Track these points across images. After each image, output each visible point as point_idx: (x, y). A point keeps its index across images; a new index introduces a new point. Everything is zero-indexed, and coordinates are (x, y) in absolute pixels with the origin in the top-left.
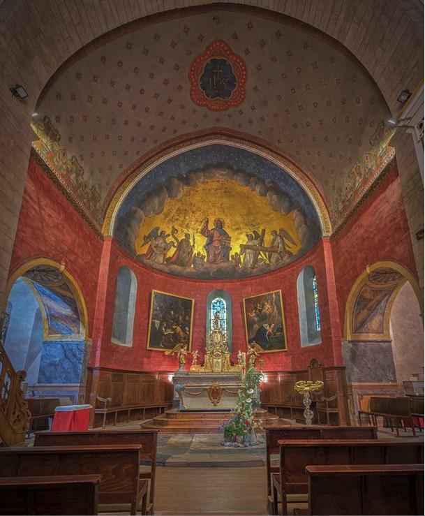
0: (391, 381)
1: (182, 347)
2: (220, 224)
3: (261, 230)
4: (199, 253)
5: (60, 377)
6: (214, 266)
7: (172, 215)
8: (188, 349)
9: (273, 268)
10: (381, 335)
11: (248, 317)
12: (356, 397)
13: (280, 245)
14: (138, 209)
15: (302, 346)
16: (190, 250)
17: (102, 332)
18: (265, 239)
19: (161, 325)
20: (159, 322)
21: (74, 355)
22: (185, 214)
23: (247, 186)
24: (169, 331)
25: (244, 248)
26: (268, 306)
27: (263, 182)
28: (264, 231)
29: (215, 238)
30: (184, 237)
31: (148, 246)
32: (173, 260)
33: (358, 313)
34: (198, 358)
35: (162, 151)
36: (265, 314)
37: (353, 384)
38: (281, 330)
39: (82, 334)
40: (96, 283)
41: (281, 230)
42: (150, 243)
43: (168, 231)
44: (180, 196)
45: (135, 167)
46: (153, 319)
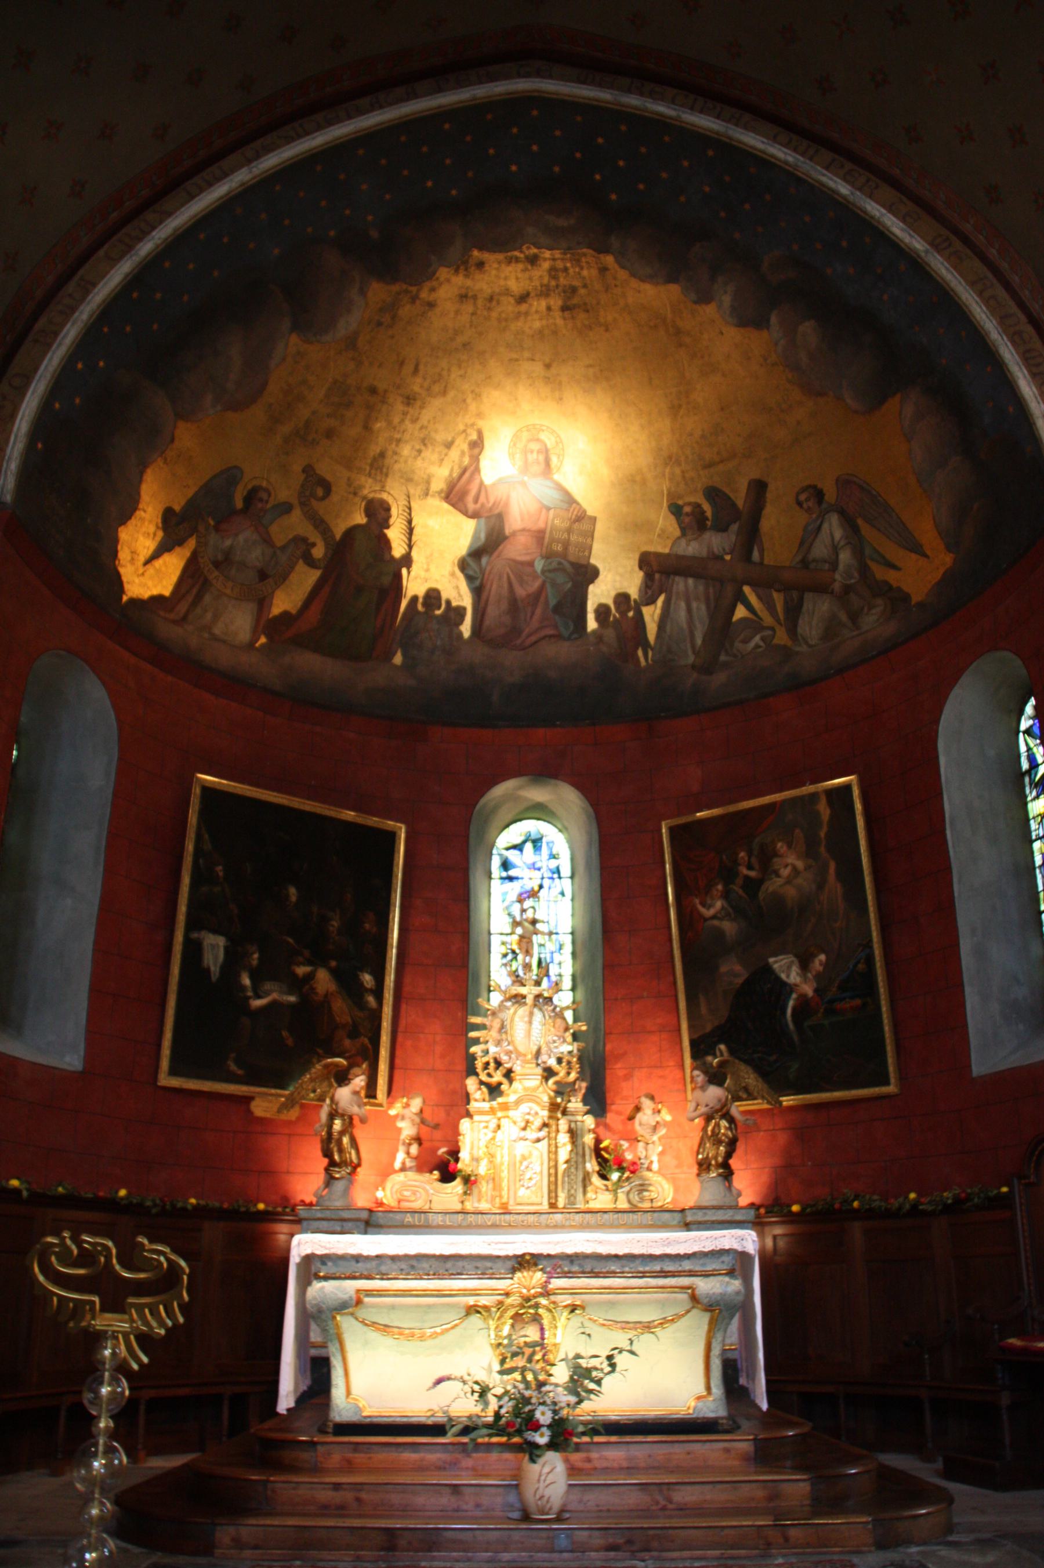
1: (343, 1078)
3: (743, 485)
4: (433, 597)
11: (688, 920)
13: (845, 557)
15: (980, 1066)
16: (386, 580)
19: (233, 960)
20: (221, 941)
23: (671, 279)
28: (759, 488)
30: (360, 519)
41: (844, 483)
44: (347, 325)
46: (192, 925)
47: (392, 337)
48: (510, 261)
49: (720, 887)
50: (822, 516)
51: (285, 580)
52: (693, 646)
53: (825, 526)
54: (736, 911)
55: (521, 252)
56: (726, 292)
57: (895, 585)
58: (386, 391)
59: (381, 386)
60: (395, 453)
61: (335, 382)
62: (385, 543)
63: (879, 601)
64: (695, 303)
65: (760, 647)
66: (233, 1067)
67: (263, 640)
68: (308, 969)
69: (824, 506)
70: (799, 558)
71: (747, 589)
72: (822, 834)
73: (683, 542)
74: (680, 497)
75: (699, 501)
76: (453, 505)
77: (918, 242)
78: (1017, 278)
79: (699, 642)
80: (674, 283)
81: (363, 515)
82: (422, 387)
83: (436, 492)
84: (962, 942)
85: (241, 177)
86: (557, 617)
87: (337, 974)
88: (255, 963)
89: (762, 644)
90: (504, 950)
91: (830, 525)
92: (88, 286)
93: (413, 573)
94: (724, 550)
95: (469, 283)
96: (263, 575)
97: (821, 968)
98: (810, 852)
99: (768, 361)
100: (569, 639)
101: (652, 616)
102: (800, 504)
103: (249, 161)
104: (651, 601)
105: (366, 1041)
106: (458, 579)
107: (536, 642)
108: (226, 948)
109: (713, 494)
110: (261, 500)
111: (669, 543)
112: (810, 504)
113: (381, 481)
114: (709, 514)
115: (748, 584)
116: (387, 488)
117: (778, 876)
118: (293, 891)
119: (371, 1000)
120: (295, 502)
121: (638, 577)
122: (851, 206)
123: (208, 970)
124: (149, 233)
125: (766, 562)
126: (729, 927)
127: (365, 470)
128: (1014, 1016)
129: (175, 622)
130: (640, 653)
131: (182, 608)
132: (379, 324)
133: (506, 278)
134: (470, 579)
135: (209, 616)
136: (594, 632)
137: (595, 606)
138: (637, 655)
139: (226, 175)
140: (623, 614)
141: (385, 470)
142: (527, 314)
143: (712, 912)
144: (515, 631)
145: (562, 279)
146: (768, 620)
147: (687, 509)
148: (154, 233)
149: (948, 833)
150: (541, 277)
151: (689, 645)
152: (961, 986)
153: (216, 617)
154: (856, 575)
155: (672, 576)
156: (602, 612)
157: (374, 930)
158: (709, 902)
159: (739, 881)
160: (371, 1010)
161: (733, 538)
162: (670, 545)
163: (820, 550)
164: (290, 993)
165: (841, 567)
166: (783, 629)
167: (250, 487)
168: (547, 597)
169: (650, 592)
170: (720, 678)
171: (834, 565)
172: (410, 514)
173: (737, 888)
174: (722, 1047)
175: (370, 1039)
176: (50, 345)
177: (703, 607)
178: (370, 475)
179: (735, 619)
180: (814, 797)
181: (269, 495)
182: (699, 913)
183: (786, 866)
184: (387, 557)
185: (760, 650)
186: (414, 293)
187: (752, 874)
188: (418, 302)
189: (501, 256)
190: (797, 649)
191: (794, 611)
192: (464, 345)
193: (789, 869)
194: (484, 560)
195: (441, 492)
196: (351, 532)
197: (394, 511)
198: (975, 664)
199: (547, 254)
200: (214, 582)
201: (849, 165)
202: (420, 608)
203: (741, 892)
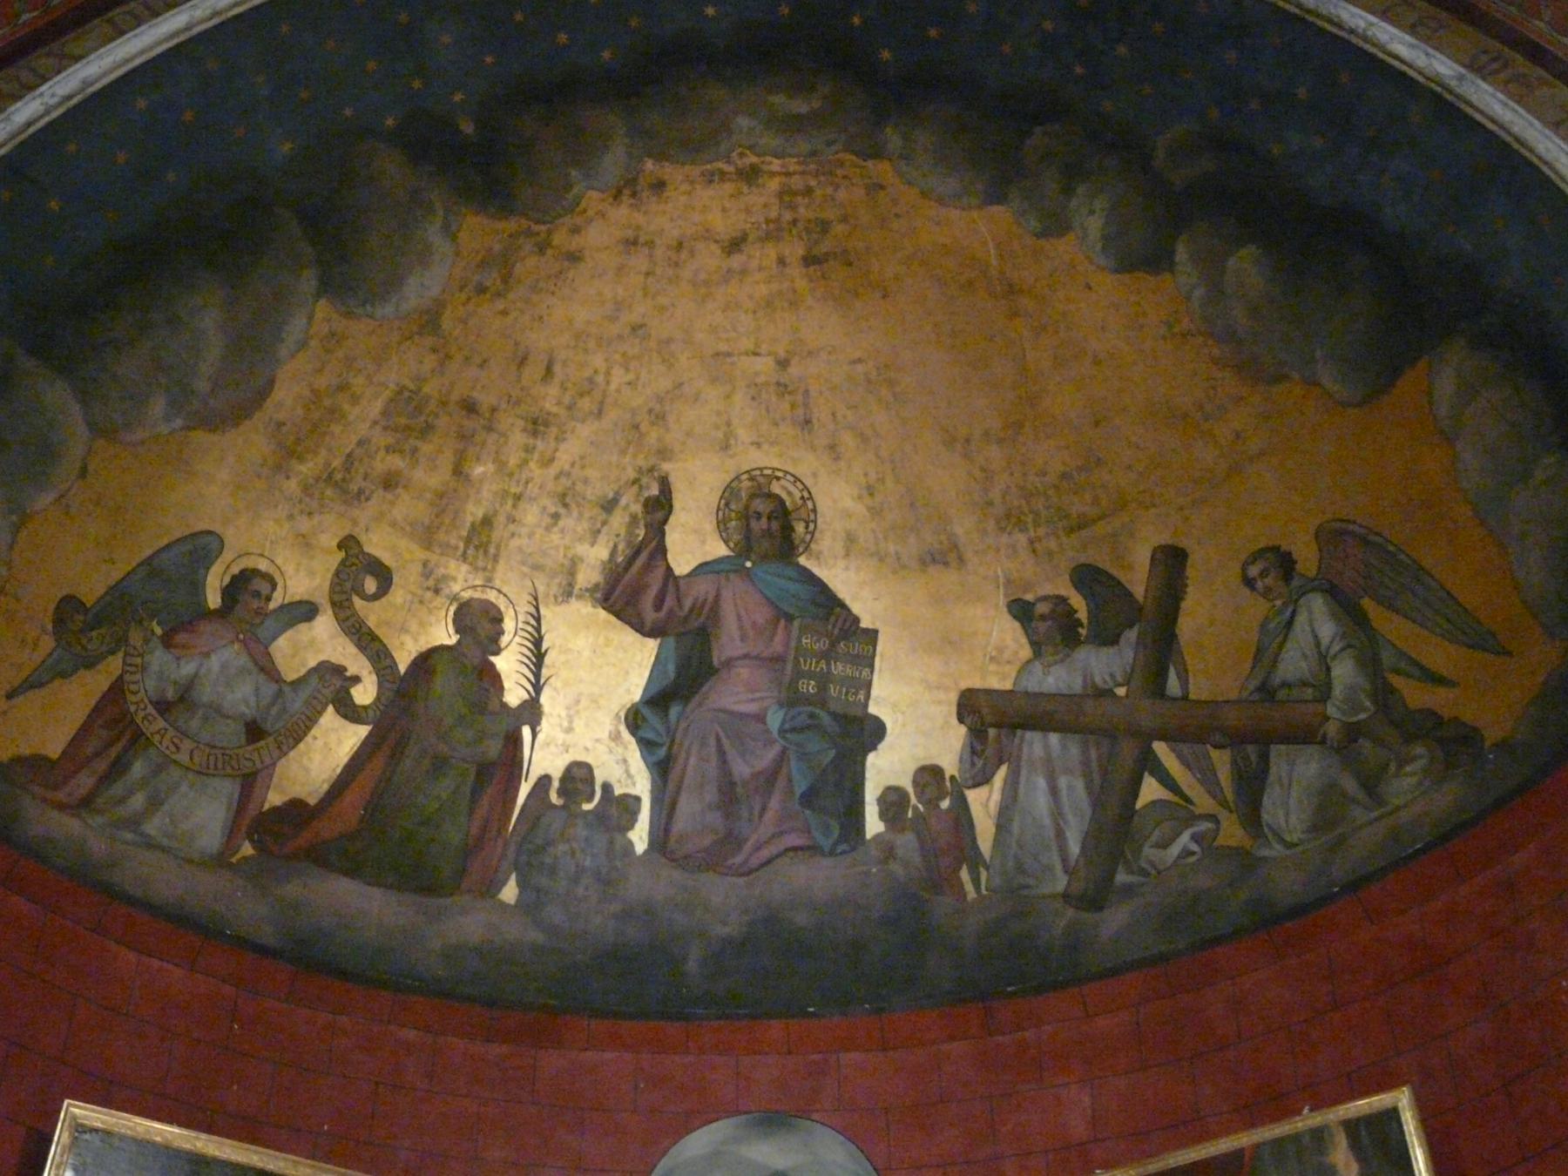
3: (1142, 556)
4: (578, 777)
7: (348, 442)
9: (1287, 884)
13: (1344, 672)
14: (27, 363)
16: (493, 748)
18: (1186, 627)
22: (464, 437)
23: (995, 195)
28: (1172, 560)
29: (729, 642)
31: (93, 684)
32: (326, 829)
41: (1332, 536)
42: (114, 665)
44: (420, 288)
47: (505, 313)
48: (710, 179)
50: (1294, 602)
52: (1064, 860)
53: (1301, 619)
55: (728, 162)
56: (1092, 212)
57: (1446, 713)
58: (494, 410)
59: (485, 400)
60: (512, 520)
61: (401, 390)
63: (1419, 749)
64: (1038, 236)
65: (1193, 853)
67: (247, 849)
69: (1296, 583)
71: (1160, 748)
73: (1038, 667)
74: (1027, 587)
75: (1063, 592)
76: (618, 615)
77: (1443, 63)
79: (1074, 849)
80: (999, 203)
81: (451, 629)
83: (587, 590)
86: (808, 812)
89: (1195, 847)
91: (1310, 612)
93: (541, 737)
94: (1112, 676)
95: (639, 218)
96: (254, 731)
99: (1176, 330)
100: (832, 853)
101: (986, 805)
102: (1249, 583)
104: (983, 779)
107: (769, 862)
109: (1088, 577)
110: (257, 594)
111: (1012, 671)
112: (1269, 581)
113: (485, 569)
114: (1082, 615)
115: (1163, 738)
116: (497, 583)
120: (323, 600)
122: (1311, 19)
125: (1192, 696)
127: (456, 548)
129: (61, 807)
130: (964, 874)
131: (84, 782)
132: (481, 290)
133: (705, 209)
134: (646, 745)
135: (138, 801)
136: (877, 837)
137: (879, 792)
138: (959, 879)
140: (932, 803)
141: (492, 550)
142: (744, 272)
144: (731, 840)
145: (802, 210)
146: (1203, 801)
147: (1042, 608)
148: (44, 88)
150: (765, 206)
153: (155, 803)
155: (1019, 732)
156: (893, 802)
161: (1129, 654)
162: (1014, 675)
163: (1294, 663)
165: (1337, 691)
166: (1234, 817)
167: (235, 570)
169: (979, 763)
170: (1114, 919)
172: (538, 629)
177: (1080, 785)
178: (464, 557)
179: (1139, 804)
180: (1319, 1136)
181: (274, 586)
184: (493, 705)
185: (1192, 859)
186: (543, 235)
188: (549, 252)
189: (695, 171)
190: (1265, 852)
191: (1251, 785)
192: (635, 329)
194: (674, 711)
195: (597, 585)
196: (426, 661)
197: (509, 625)
199: (776, 165)
200: (157, 738)
202: (554, 798)
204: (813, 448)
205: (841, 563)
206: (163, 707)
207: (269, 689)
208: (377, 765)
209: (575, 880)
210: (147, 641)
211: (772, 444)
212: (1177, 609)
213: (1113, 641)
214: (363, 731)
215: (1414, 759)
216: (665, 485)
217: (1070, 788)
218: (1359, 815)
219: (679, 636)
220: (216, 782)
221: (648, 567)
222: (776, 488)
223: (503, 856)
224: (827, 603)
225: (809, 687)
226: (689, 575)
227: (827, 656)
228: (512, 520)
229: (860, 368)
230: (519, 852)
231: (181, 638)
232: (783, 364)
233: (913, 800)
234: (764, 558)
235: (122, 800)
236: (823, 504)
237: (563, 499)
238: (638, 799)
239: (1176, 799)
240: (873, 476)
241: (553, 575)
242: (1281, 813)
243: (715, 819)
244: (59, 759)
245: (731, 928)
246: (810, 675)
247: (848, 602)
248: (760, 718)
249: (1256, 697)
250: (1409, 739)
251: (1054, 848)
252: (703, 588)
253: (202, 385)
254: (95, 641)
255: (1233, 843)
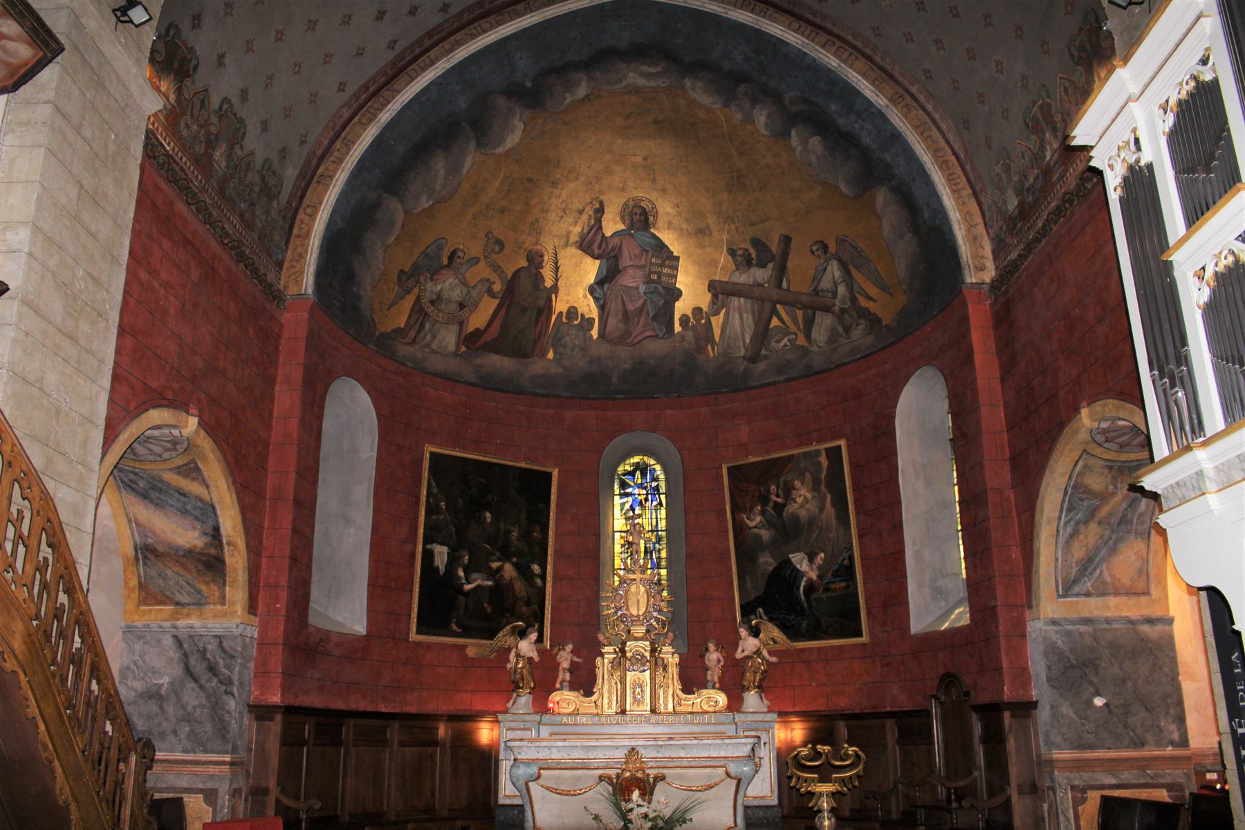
0: (1172, 743)
1: (522, 634)
2: (640, 218)
3: (776, 239)
4: (572, 312)
5: (175, 732)
6: (623, 352)
8: (540, 639)
10: (1143, 599)
11: (739, 529)
12: (1065, 798)
13: (842, 289)
14: (385, 195)
16: (541, 303)
17: (284, 595)
19: (453, 560)
20: (445, 549)
21: (212, 669)
24: (480, 580)
25: (720, 292)
26: (802, 493)
27: (775, 97)
28: (787, 240)
29: (625, 261)
31: (408, 303)
32: (487, 338)
33: (1072, 536)
34: (573, 668)
35: (463, 27)
36: (795, 517)
37: (1057, 755)
38: (847, 572)
39: (233, 604)
40: (266, 445)
41: (841, 241)
42: (416, 291)
43: (475, 249)
45: (383, 80)
46: (428, 539)
49: (759, 508)
50: (827, 261)
51: (476, 307)
52: (744, 344)
53: (829, 268)
54: (769, 524)
56: (761, 115)
60: (545, 219)
62: (539, 278)
63: (863, 321)
66: (454, 627)
67: (463, 349)
68: (499, 564)
69: (828, 255)
70: (812, 288)
71: (778, 306)
72: (823, 476)
73: (737, 274)
78: (944, 126)
79: (748, 341)
82: (562, 175)
84: (906, 550)
85: (442, 66)
86: (654, 324)
87: (517, 566)
88: (466, 562)
89: (789, 344)
90: (622, 542)
91: (832, 268)
92: (348, 145)
96: (462, 306)
97: (821, 562)
98: (815, 488)
100: (663, 338)
102: (813, 252)
103: (448, 52)
104: (717, 313)
105: (536, 607)
106: (589, 300)
108: (448, 553)
109: (756, 242)
110: (459, 257)
112: (819, 252)
115: (780, 304)
116: (540, 242)
117: (795, 502)
118: (488, 515)
119: (539, 581)
121: (708, 297)
123: (437, 569)
124: (386, 105)
126: (765, 534)
128: (829, 690)
129: (407, 344)
130: (709, 347)
131: (412, 334)
134: (596, 299)
135: (429, 337)
136: (678, 333)
139: (433, 63)
140: (698, 321)
143: (754, 523)
144: (627, 334)
146: (792, 328)
147: (739, 252)
149: (900, 479)
151: (741, 343)
152: (905, 577)
153: (434, 337)
154: (848, 302)
156: (684, 320)
157: (540, 536)
158: (752, 517)
159: (771, 504)
160: (539, 587)
163: (825, 283)
164: (488, 580)
165: (839, 296)
167: (452, 250)
168: (648, 311)
170: (761, 366)
171: (835, 295)
172: (556, 259)
173: (769, 509)
174: (761, 610)
175: (538, 606)
176: (328, 186)
177: (750, 317)
179: (771, 326)
180: (818, 452)
182: (747, 525)
183: (800, 496)
184: (542, 287)
187: (779, 500)
190: (811, 349)
191: (809, 323)
193: (802, 498)
194: (606, 286)
195: (577, 242)
196: (517, 274)
197: (546, 258)
198: (919, 371)
201: (838, 44)
202: (564, 320)
203: (772, 511)
204: (656, 190)
205: (667, 231)
206: (432, 302)
207: (465, 290)
208: (503, 312)
209: (573, 350)
210: (425, 280)
211: (641, 188)
212: (787, 258)
213: (765, 266)
214: (497, 301)
215: (860, 324)
216: (601, 203)
217: (747, 318)
218: (842, 340)
219: (608, 259)
220: (451, 326)
221: (596, 234)
222: (643, 204)
223: (548, 342)
224: (661, 247)
225: (655, 277)
226: (611, 236)
227: (662, 265)
228: (545, 219)
229: (674, 161)
230: (552, 341)
231: (435, 277)
232: (645, 159)
233: (692, 320)
234: (638, 230)
235: (424, 338)
236: (660, 210)
237: (564, 211)
238: (594, 319)
239: (782, 325)
240: (678, 201)
241: (560, 239)
242: (818, 335)
243: (621, 326)
244: (775, 712)
245: (627, 366)
246: (655, 273)
247: (669, 246)
248: (637, 288)
249: (813, 293)
250: (860, 317)
251: (741, 339)
252: (616, 241)
253: (438, 187)
254: (410, 283)
255: (801, 344)
